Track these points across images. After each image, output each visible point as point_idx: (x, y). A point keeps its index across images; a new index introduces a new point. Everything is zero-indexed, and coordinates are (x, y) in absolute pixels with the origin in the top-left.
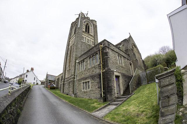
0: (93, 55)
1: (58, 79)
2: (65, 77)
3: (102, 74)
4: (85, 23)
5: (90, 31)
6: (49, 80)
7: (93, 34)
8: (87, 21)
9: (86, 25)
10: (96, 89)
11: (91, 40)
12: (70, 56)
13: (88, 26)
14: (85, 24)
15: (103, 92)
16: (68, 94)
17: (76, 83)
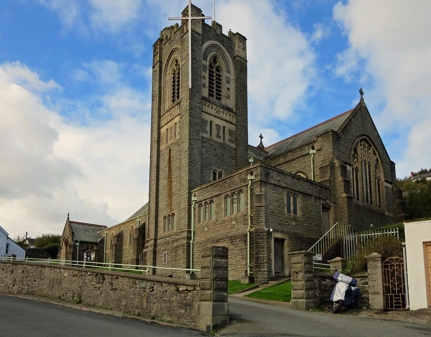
0: (234, 193)
1: (120, 237)
2: (156, 235)
3: (250, 235)
4: (205, 59)
5: (224, 92)
6: (81, 242)
7: (231, 103)
8: (214, 46)
9: (210, 66)
10: (238, 261)
11: (228, 125)
12: (170, 177)
13: (218, 69)
14: (207, 63)
15: (250, 267)
16: (171, 276)
17: (193, 250)
